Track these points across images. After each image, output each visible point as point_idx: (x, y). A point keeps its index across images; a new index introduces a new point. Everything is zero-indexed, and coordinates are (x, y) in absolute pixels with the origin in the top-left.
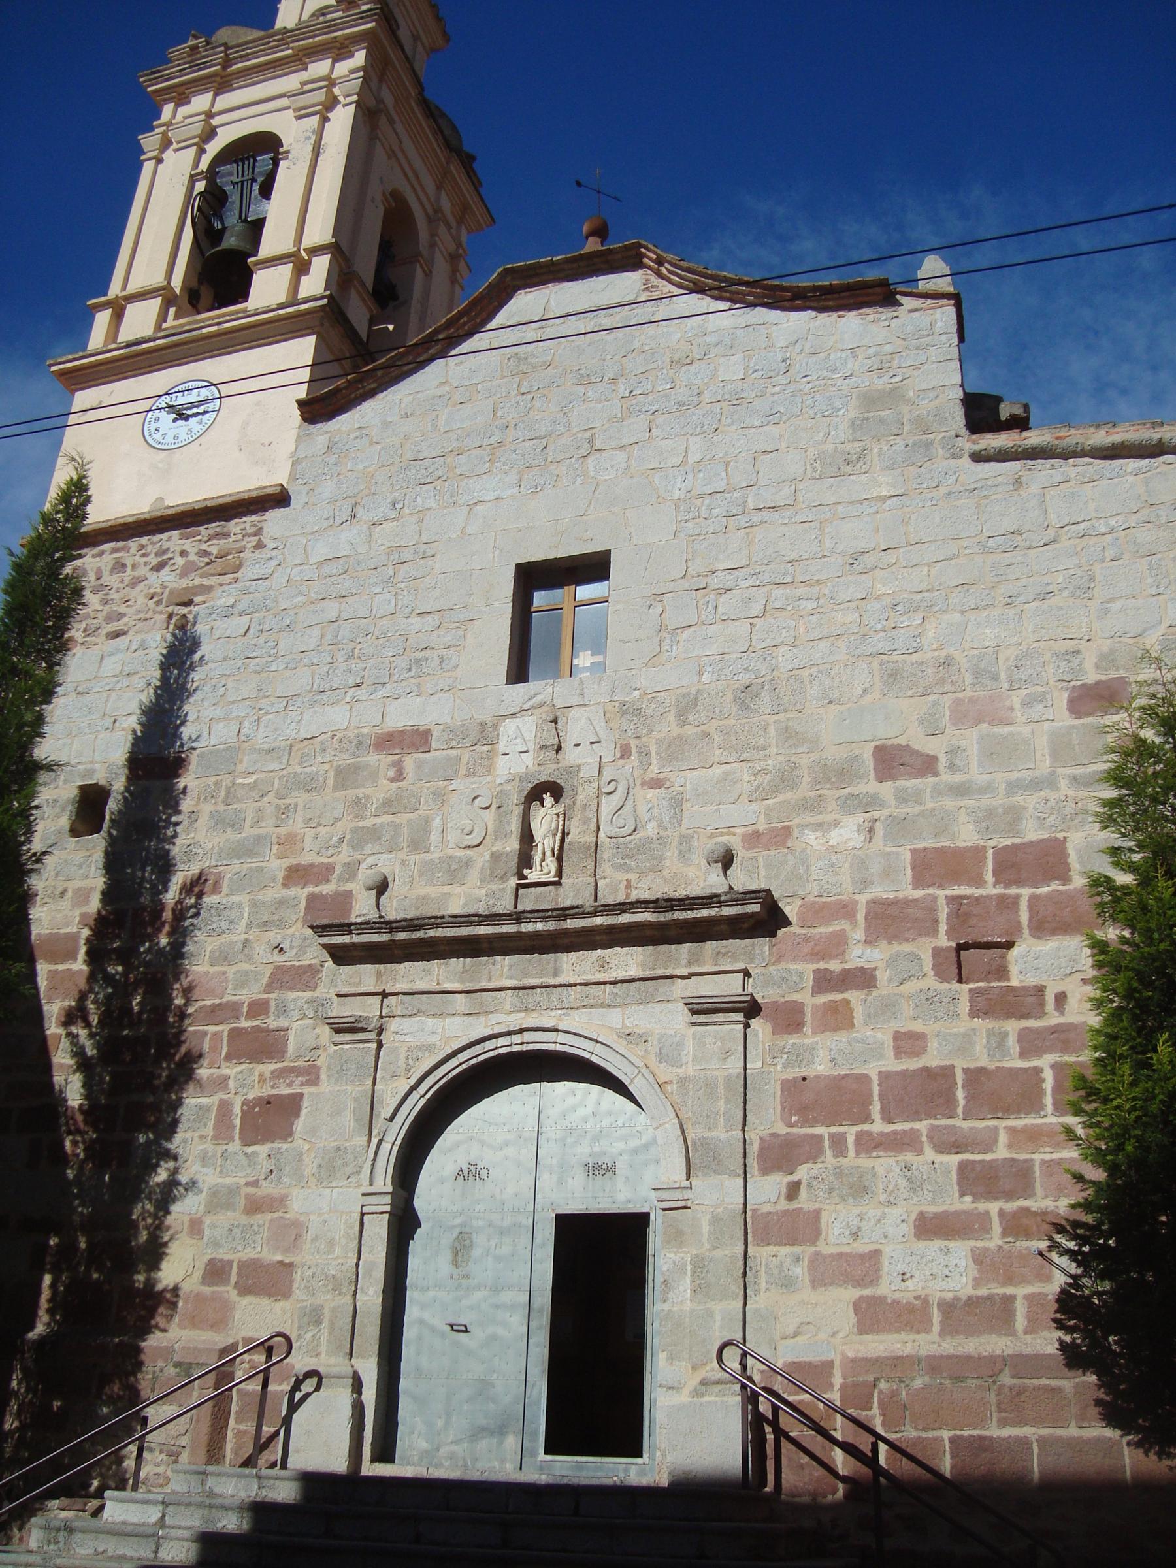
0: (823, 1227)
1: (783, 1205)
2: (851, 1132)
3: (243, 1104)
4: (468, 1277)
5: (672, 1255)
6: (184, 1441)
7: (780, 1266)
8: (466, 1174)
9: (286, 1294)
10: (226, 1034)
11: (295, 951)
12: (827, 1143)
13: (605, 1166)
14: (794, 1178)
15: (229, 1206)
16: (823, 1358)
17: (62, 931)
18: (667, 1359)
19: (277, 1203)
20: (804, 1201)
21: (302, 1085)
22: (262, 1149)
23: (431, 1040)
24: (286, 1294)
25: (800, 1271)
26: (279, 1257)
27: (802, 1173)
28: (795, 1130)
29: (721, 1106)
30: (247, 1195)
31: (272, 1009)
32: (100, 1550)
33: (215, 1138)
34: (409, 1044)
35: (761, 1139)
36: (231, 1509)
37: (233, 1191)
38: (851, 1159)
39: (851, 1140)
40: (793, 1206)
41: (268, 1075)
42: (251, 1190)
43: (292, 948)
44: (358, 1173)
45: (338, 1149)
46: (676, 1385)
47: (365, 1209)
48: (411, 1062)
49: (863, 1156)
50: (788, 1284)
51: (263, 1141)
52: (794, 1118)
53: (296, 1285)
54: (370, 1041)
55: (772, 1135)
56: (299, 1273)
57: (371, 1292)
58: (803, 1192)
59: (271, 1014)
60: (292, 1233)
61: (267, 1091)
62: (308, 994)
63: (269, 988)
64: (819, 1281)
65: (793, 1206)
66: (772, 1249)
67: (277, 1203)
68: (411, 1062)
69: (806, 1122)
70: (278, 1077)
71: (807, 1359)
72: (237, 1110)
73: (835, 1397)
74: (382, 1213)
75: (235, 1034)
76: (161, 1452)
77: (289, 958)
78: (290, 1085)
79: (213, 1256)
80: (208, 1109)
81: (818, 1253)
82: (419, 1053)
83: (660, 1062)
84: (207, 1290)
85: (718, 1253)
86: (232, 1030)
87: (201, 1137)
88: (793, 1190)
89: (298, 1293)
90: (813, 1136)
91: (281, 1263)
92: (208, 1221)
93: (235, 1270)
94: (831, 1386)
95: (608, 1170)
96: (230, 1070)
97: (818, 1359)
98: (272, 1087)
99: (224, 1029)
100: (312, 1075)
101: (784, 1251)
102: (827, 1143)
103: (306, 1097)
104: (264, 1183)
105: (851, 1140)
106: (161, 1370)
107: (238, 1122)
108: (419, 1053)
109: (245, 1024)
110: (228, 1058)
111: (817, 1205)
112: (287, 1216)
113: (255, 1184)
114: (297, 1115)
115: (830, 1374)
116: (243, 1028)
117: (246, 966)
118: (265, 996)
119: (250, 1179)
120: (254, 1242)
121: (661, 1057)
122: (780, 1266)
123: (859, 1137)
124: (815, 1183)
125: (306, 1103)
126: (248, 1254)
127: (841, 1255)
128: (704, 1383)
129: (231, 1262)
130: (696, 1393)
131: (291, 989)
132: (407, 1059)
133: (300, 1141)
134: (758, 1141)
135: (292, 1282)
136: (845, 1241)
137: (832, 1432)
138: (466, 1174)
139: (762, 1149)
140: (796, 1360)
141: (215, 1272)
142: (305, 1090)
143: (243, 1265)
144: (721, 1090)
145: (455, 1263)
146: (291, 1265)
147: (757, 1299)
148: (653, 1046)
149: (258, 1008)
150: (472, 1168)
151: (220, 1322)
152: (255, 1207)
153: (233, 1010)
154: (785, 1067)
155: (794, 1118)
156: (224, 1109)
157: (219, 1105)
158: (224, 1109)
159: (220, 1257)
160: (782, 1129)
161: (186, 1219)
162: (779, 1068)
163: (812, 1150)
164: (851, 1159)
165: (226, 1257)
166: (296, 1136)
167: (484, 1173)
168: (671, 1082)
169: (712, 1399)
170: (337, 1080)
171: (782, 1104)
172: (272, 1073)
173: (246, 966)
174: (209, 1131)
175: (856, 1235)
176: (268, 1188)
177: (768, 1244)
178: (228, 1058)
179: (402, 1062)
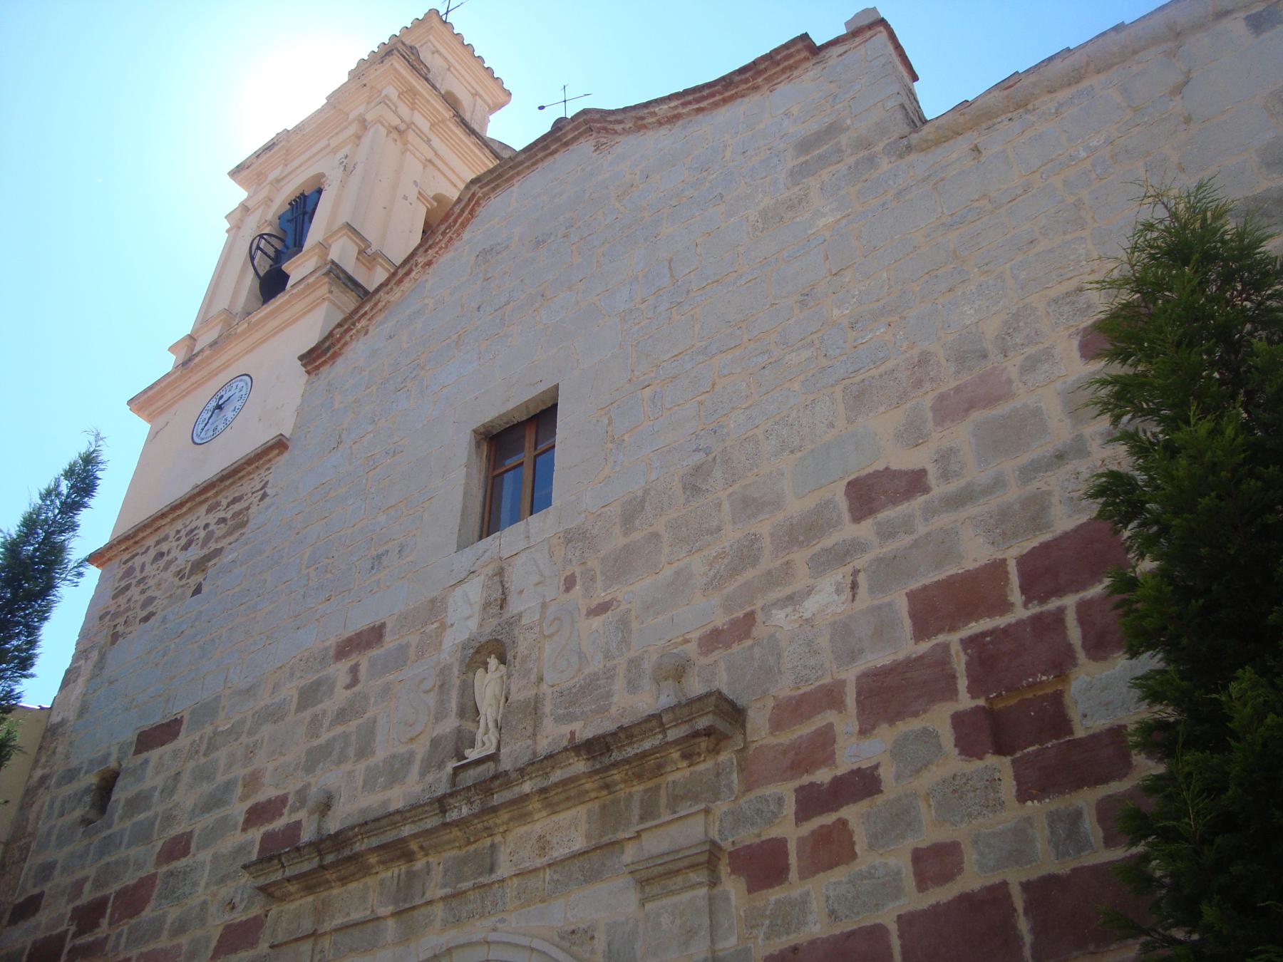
17: (54, 933)
43: (242, 900)
77: (239, 916)
129: (805, 874)
154: (767, 937)
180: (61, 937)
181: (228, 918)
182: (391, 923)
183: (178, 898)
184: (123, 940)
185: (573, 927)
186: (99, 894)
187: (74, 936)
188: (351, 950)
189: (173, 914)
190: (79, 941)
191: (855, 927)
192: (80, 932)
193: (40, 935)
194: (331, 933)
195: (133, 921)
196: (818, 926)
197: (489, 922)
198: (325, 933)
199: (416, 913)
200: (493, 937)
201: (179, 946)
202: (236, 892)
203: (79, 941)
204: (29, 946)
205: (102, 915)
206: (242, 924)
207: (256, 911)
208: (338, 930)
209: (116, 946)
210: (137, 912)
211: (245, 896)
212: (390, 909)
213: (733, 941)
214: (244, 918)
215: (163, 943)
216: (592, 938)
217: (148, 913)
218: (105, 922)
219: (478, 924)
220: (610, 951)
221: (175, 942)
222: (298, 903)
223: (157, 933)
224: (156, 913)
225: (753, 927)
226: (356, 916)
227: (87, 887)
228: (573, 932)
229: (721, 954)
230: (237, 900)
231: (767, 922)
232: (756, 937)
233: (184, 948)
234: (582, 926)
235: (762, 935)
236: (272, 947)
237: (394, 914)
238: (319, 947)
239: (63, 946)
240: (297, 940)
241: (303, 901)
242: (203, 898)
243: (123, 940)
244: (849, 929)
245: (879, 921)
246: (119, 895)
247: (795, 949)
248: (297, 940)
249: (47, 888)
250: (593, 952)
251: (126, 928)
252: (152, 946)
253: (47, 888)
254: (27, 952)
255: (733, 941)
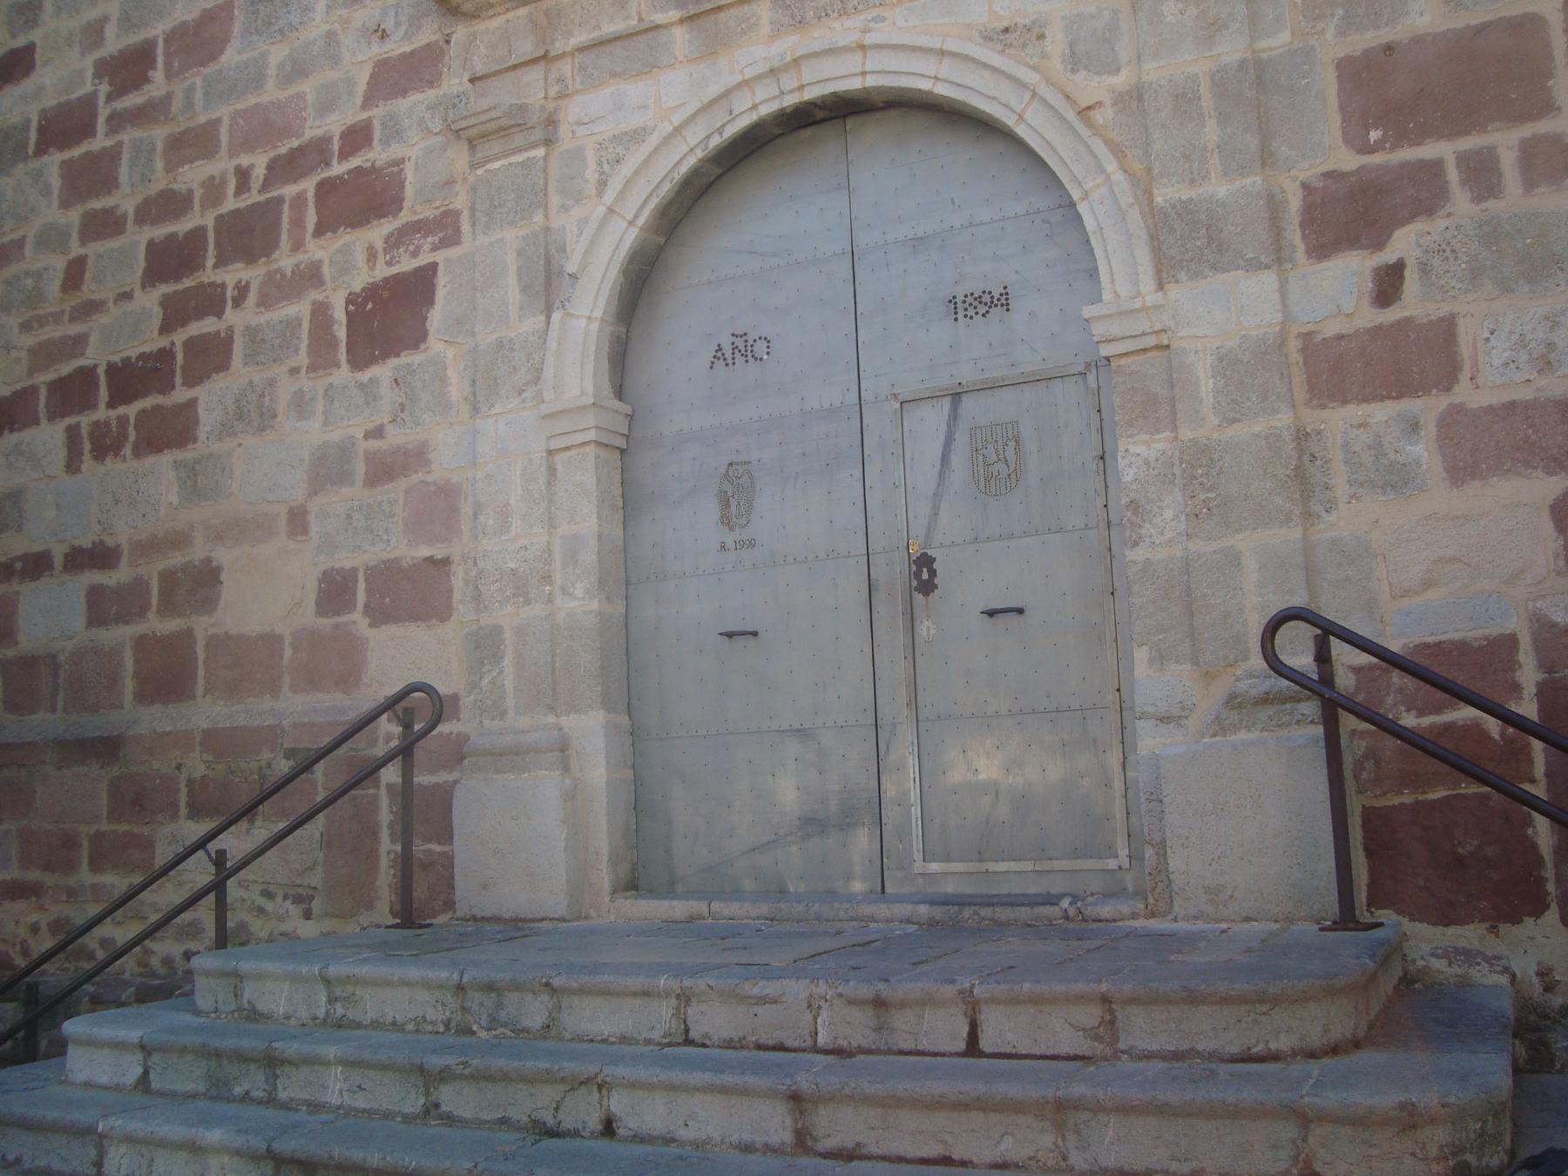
0: (1465, 350)
1: (1371, 316)
2: (1505, 142)
3: (347, 304)
4: (752, 544)
5: (1141, 449)
6: (316, 879)
7: (1377, 447)
8: (728, 355)
9: (442, 613)
10: (311, 195)
11: (403, 28)
12: (1453, 175)
13: (986, 298)
14: (1389, 256)
15: (344, 478)
16: (1493, 631)
17: (73, 97)
18: (1151, 661)
19: (417, 457)
20: (1414, 303)
21: (435, 249)
22: (381, 372)
23: (636, 121)
24: (442, 613)
25: (1422, 451)
26: (425, 552)
27: (1404, 243)
28: (1378, 158)
29: (1211, 133)
30: (366, 453)
31: (377, 135)
32: (11, 1157)
33: (312, 368)
34: (599, 138)
35: (1305, 186)
36: (256, 1061)
37: (345, 450)
38: (1513, 197)
39: (1508, 160)
40: (1391, 315)
41: (379, 245)
42: (374, 444)
43: (398, 24)
44: (537, 380)
45: (501, 344)
46: (1175, 712)
47: (554, 445)
48: (606, 168)
49: (1543, 189)
50: (1397, 480)
51: (385, 355)
52: (1374, 135)
53: (456, 596)
54: (533, 146)
55: (1328, 175)
56: (460, 574)
57: (579, 591)
58: (1411, 284)
59: (375, 142)
60: (440, 508)
61: (382, 271)
62: (431, 94)
63: (369, 100)
64: (1464, 466)
65: (1391, 315)
66: (1355, 411)
67: (417, 457)
68: (606, 168)
69: (1401, 137)
70: (397, 245)
71: (1457, 636)
72: (340, 315)
73: (1528, 708)
74: (584, 444)
75: (326, 189)
76: (285, 897)
77: (396, 47)
78: (415, 254)
79: (329, 565)
80: (293, 324)
81: (1456, 410)
82: (620, 149)
83: (1074, 71)
84: (326, 623)
85: (1237, 432)
86: (321, 185)
87: (294, 371)
88: (1388, 284)
89: (463, 610)
90: (1422, 165)
91: (430, 560)
92: (314, 506)
93: (362, 585)
94: (1516, 688)
95: (992, 304)
96: (319, 251)
97: (1479, 633)
98: (390, 264)
99: (308, 185)
100: (446, 228)
101: (1381, 412)
102: (1453, 175)
103: (441, 269)
104: (390, 430)
105: (1508, 160)
106: (269, 765)
107: (341, 333)
108: (620, 149)
109: (338, 169)
110: (319, 232)
111: (1445, 309)
112: (430, 478)
113: (377, 433)
114: (430, 302)
115: (1512, 664)
116: (338, 177)
117: (332, 75)
118: (365, 115)
119: (370, 426)
120: (387, 531)
121: (1074, 61)
122: (1377, 447)
123: (1528, 152)
124: (1436, 262)
125: (442, 279)
126: (375, 554)
127: (1512, 405)
128: (1234, 702)
129: (354, 570)
130: (1220, 727)
131: (403, 93)
132: (600, 164)
133: (441, 346)
134: (1300, 193)
135: (450, 591)
136: (1519, 377)
137: (1526, 787)
138: (728, 355)
139: (1308, 207)
140: (1430, 639)
141: (335, 591)
142: (440, 256)
143: (373, 572)
144: (1207, 103)
145: (726, 521)
146: (446, 561)
147: (1332, 517)
148: (1056, 42)
149: (357, 138)
150: (740, 343)
151: (348, 679)
152: (384, 470)
153: (317, 152)
154: (1341, 33)
155: (1374, 135)
156: (321, 314)
157: (313, 314)
158: (321, 314)
159: (338, 565)
160: (1348, 161)
161: (284, 510)
162: (1329, 36)
163: (1421, 192)
164: (1513, 197)
165: (347, 564)
166: (431, 339)
167: (760, 348)
168: (1100, 104)
169: (1255, 735)
170: (487, 227)
171: (1342, 109)
172: (387, 240)
173: (332, 75)
174: (302, 358)
175: (1545, 364)
176: (396, 437)
177: (1345, 402)
178: (319, 232)
179: (591, 174)
180: (89, 102)
181: (378, 50)
182: (679, 32)
183: (281, 31)
184: (199, 94)
185: (1005, 24)
186: (135, 38)
187: (110, 98)
188: (613, 75)
189: (277, 54)
190: (120, 105)
191: (1489, 18)
192: (119, 91)
193: (50, 102)
194: (572, 54)
195: (211, 69)
196: (1427, 18)
197: (856, 22)
198: (564, 55)
199: (722, 16)
200: (869, 39)
201: (301, 96)
202: (384, 13)
203: (120, 105)
204: (35, 119)
205: (152, 64)
206: (403, 56)
207: (427, 35)
208: (582, 49)
209: (189, 105)
210: (213, 57)
211: (403, 19)
212: (674, 15)
213: (1284, 37)
214: (408, 49)
215: (271, 93)
216: (1041, 37)
217: (231, 56)
218: (158, 75)
219: (837, 25)
220: (1073, 54)
221: (292, 91)
222: (503, 18)
223: (257, 81)
224: (244, 57)
225: (1317, 18)
226: (609, 28)
227: (110, 31)
228: (1006, 30)
229: (1264, 55)
230: (389, 25)
231: (1340, 11)
232: (1323, 32)
233: (310, 99)
234: (1022, 21)
235: (1331, 30)
236: (472, 81)
237: (681, 21)
238: (553, 76)
239: (94, 116)
240: (515, 67)
241: (510, 16)
242: (326, 27)
243: (199, 94)
244: (1479, 21)
245: (1531, 9)
246: (169, 38)
247: (1389, 49)
248: (515, 67)
249: (36, 36)
250: (1044, 55)
251: (198, 81)
252: (252, 100)
253: (36, 36)
254: (34, 126)
255: (1284, 37)
